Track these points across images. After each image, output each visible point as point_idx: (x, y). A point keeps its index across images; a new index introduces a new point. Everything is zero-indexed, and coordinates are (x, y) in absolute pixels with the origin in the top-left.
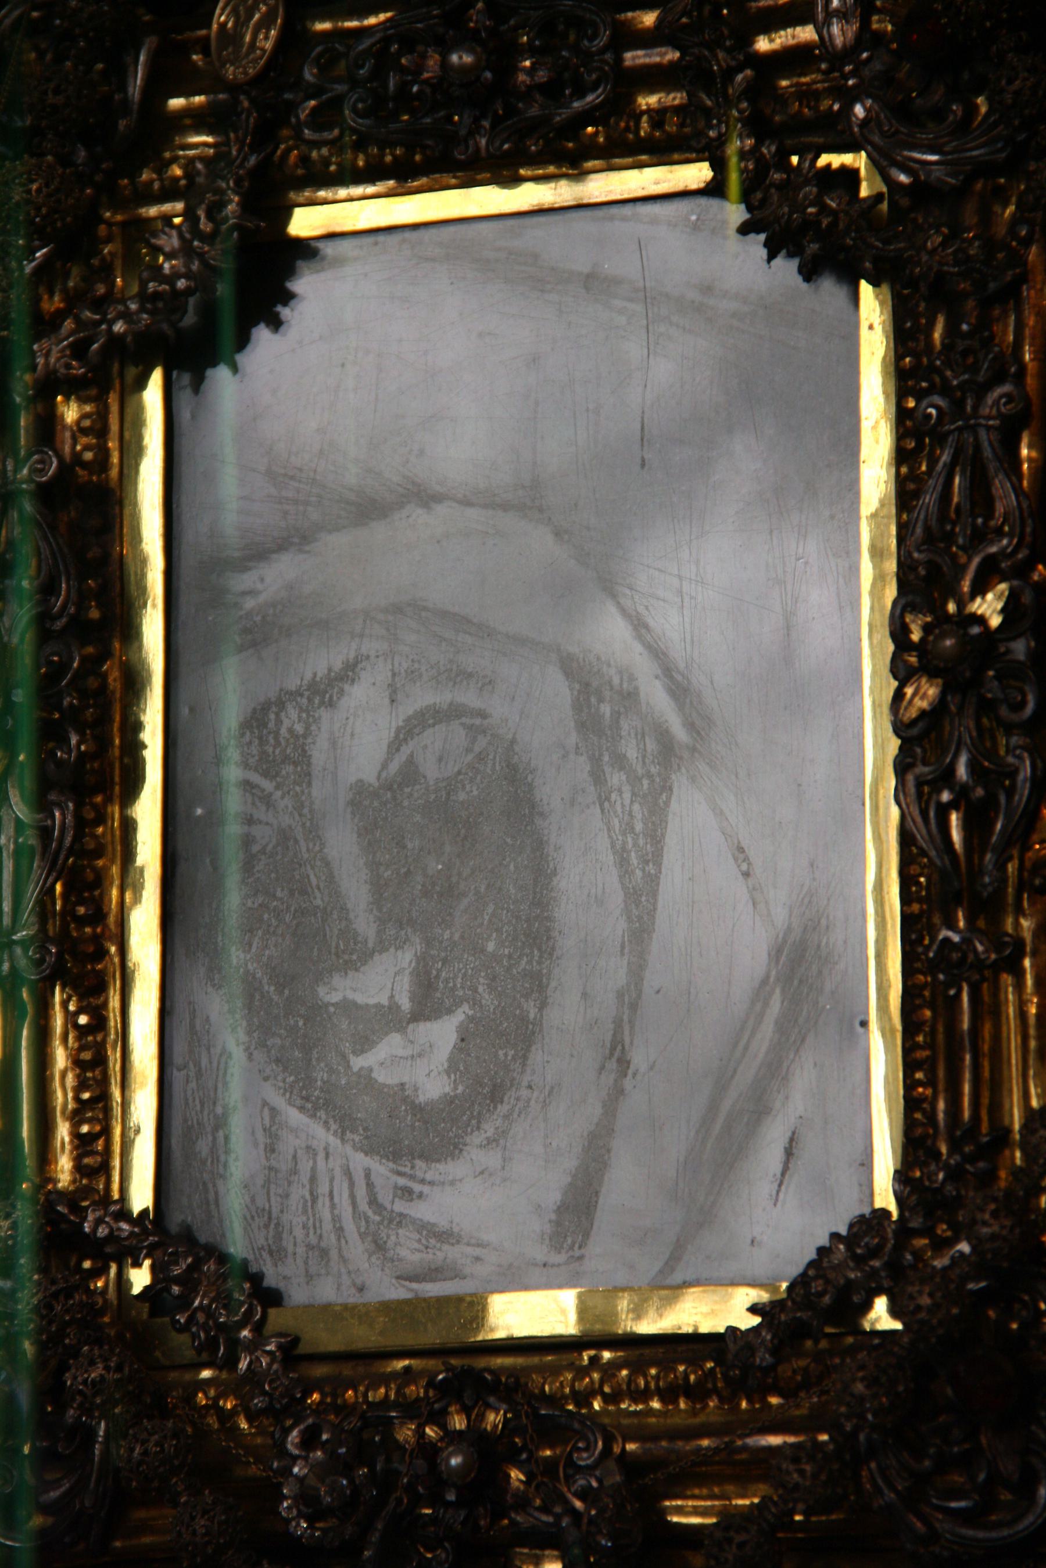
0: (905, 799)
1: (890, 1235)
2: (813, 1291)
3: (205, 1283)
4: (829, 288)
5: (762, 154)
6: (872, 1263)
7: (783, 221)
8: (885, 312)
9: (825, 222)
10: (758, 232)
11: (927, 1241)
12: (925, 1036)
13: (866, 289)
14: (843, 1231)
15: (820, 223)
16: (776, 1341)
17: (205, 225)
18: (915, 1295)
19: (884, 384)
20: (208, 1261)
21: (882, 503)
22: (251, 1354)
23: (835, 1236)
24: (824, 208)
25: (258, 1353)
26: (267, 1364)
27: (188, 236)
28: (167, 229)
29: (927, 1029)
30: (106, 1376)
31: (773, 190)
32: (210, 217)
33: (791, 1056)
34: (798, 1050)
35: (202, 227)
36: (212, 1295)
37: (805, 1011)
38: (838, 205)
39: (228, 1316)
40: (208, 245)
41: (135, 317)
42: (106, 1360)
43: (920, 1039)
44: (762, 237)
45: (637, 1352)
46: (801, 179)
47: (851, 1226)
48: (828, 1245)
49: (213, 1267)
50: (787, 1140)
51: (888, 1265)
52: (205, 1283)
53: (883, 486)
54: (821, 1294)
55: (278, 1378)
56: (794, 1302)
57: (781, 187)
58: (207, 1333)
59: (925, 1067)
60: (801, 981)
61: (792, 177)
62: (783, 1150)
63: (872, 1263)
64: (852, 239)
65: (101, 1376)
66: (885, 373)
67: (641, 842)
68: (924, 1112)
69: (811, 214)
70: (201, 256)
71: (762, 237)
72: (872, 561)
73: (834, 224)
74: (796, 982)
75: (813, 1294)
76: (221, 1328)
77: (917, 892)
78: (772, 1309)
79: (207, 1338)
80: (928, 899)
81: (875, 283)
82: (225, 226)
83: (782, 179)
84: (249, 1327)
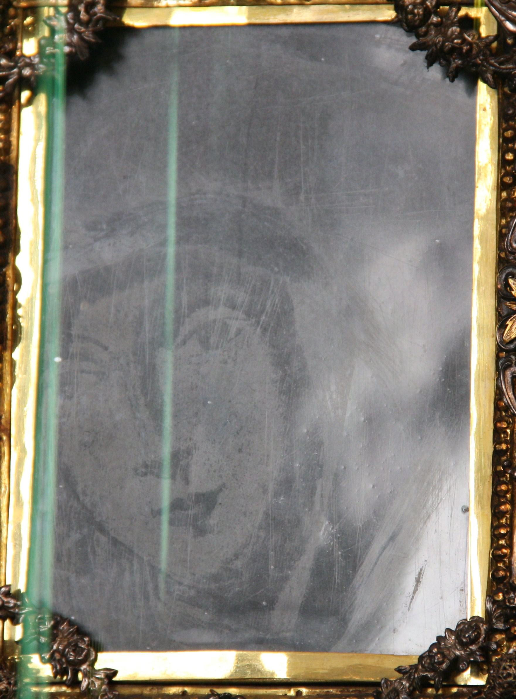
0: (505, 386)
1: (483, 632)
2: (436, 661)
3: (61, 636)
4: (460, 85)
5: (427, 5)
6: (471, 647)
7: (439, 46)
8: (493, 102)
9: (465, 48)
10: (422, 50)
11: (503, 636)
12: (506, 520)
13: (482, 86)
14: (454, 628)
15: (461, 49)
16: (411, 688)
17: (83, 16)
18: (507, 667)
19: (491, 142)
20: (63, 623)
21: (488, 211)
22: (89, 678)
23: (448, 630)
24: (464, 40)
25: (93, 679)
26: (99, 686)
27: (71, 21)
28: (57, 15)
29: (508, 516)
30: (9, 688)
31: (432, 27)
32: (87, 11)
33: (421, 526)
34: (425, 522)
35: (82, 17)
36: (65, 643)
37: (431, 500)
38: (472, 39)
39: (75, 656)
40: (85, 28)
41: (36, 66)
42: (8, 679)
43: (504, 521)
44: (425, 53)
45: (325, 690)
46: (449, 22)
47: (458, 626)
48: (443, 635)
49: (66, 628)
50: (417, 574)
51: (481, 649)
52: (61, 636)
53: (489, 203)
54: (441, 663)
55: (106, 694)
56: (423, 666)
57: (437, 25)
58: (61, 665)
59: (506, 537)
60: (429, 484)
61: (444, 20)
62: (414, 579)
63: (471, 647)
64: (480, 60)
65: (6, 688)
66: (492, 137)
67: (334, 396)
68: (504, 563)
69: (457, 43)
70: (79, 34)
71: (425, 53)
72: (481, 245)
73: (470, 50)
74: (425, 484)
75: (436, 663)
76: (69, 662)
77: (504, 437)
78: (410, 669)
79: (61, 668)
80: (511, 442)
81: (493, 85)
82: (95, 17)
83: (438, 21)
84: (87, 663)
